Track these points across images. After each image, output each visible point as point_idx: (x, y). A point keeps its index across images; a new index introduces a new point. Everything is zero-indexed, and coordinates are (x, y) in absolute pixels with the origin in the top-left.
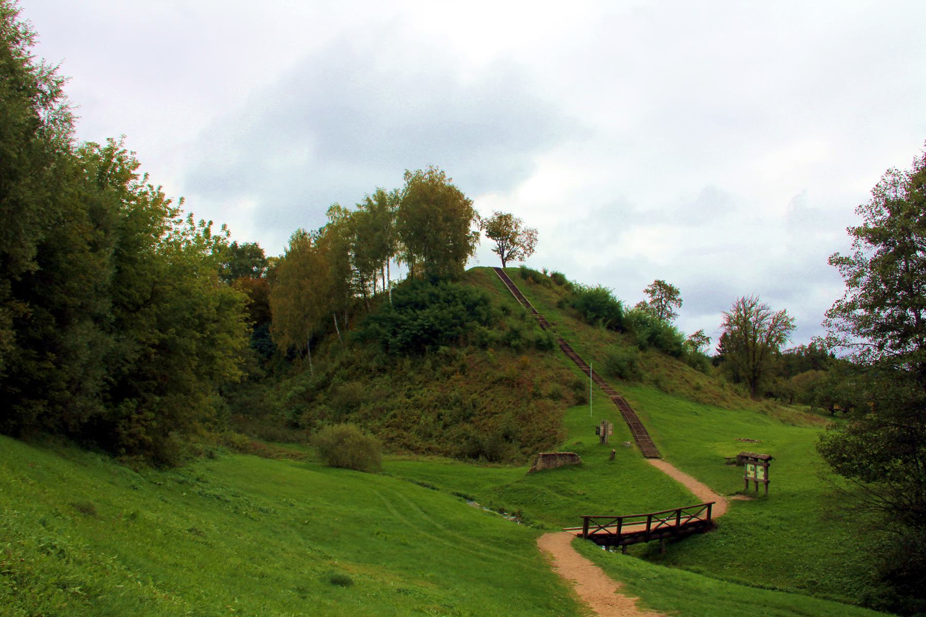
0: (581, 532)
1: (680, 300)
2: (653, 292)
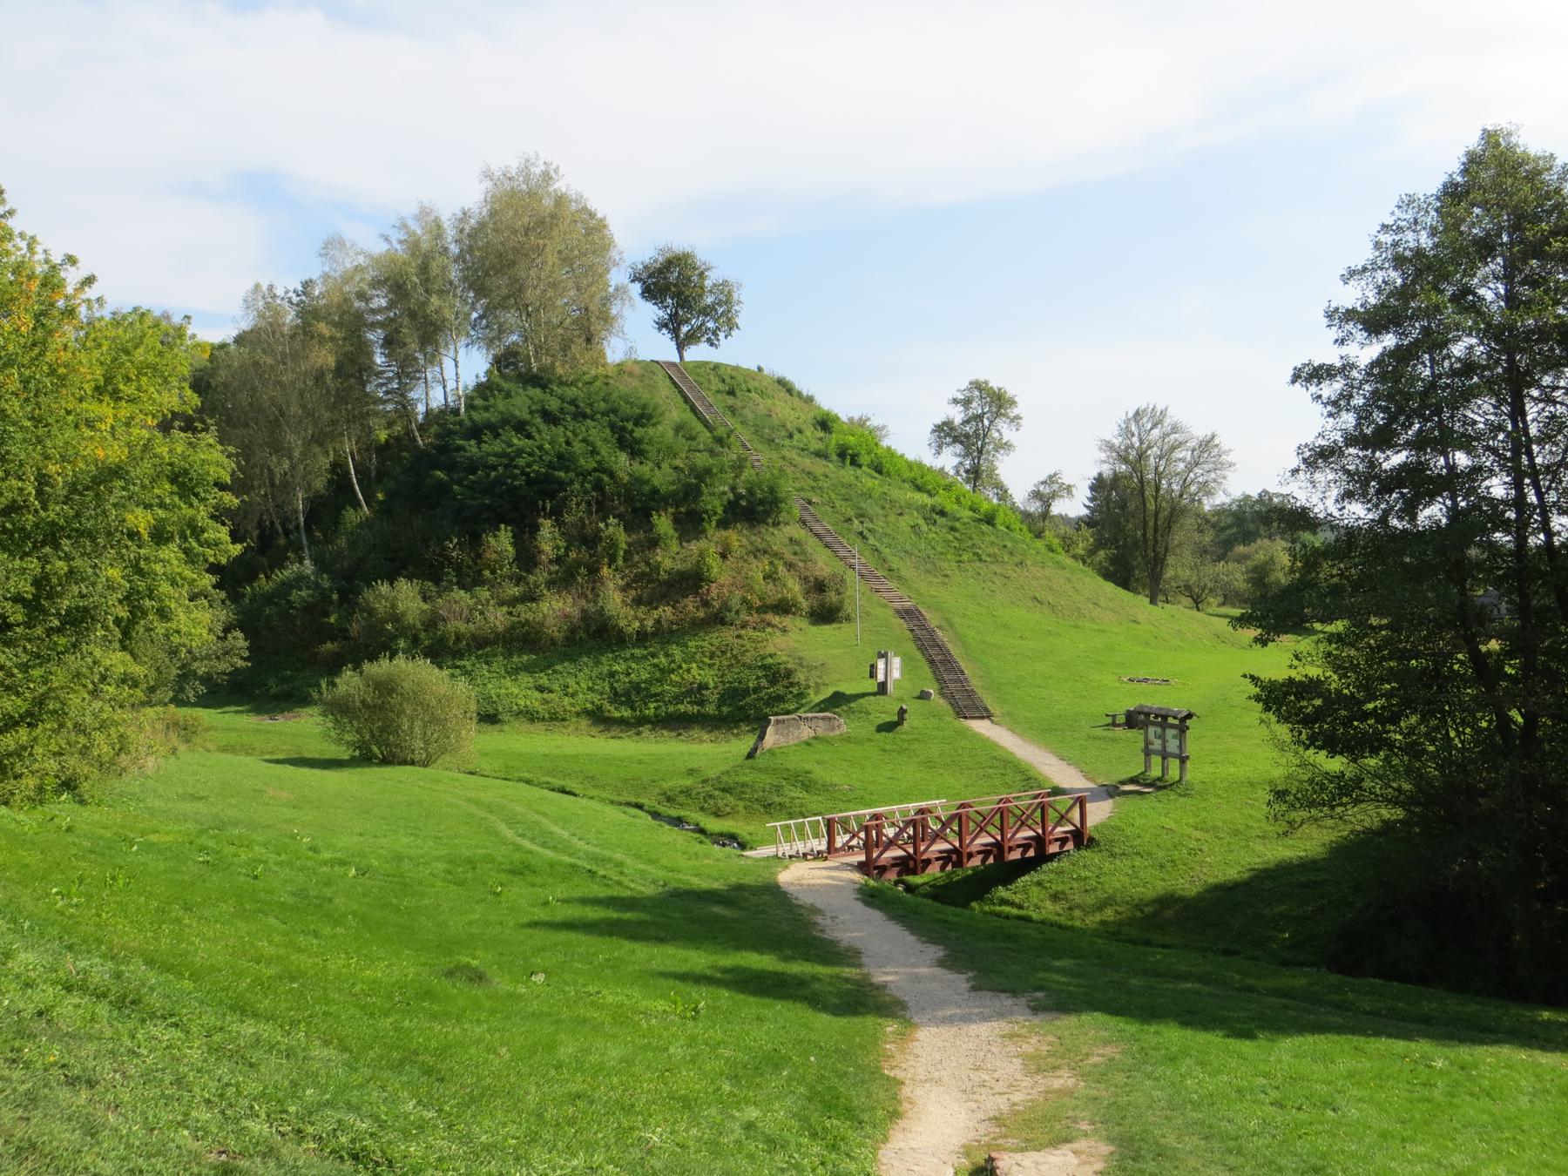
0: (863, 858)
1: (1018, 417)
2: (967, 403)
